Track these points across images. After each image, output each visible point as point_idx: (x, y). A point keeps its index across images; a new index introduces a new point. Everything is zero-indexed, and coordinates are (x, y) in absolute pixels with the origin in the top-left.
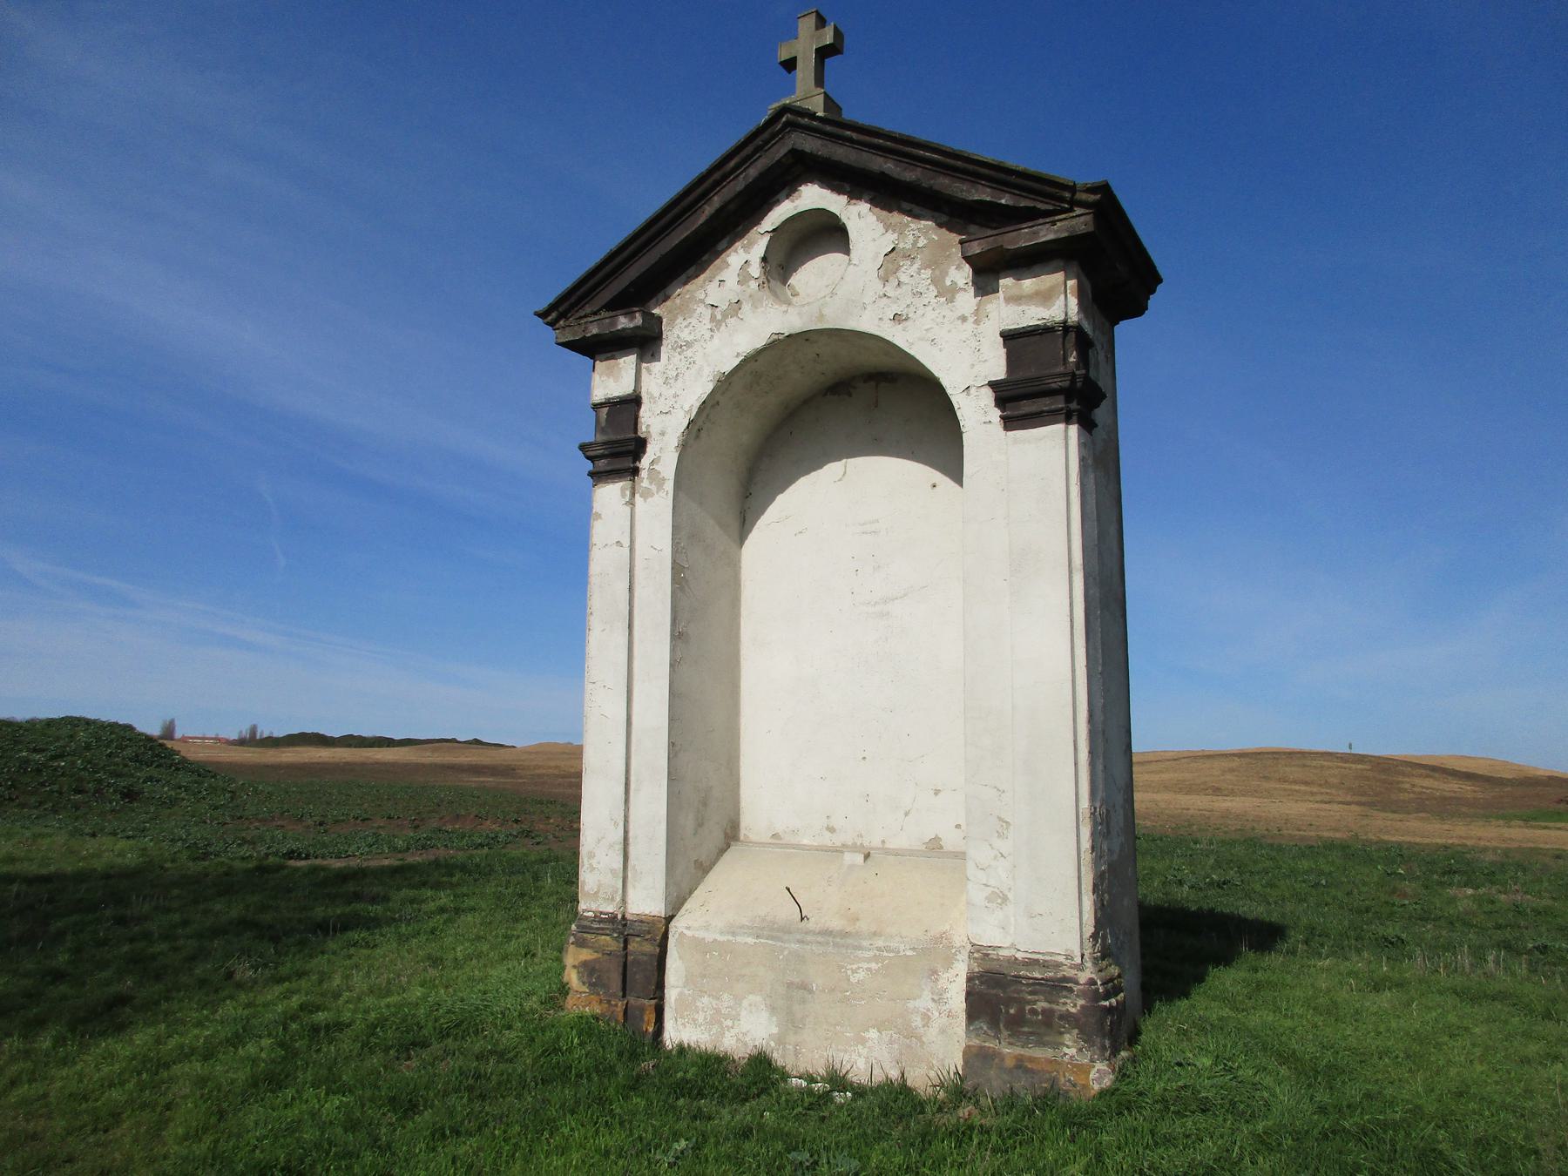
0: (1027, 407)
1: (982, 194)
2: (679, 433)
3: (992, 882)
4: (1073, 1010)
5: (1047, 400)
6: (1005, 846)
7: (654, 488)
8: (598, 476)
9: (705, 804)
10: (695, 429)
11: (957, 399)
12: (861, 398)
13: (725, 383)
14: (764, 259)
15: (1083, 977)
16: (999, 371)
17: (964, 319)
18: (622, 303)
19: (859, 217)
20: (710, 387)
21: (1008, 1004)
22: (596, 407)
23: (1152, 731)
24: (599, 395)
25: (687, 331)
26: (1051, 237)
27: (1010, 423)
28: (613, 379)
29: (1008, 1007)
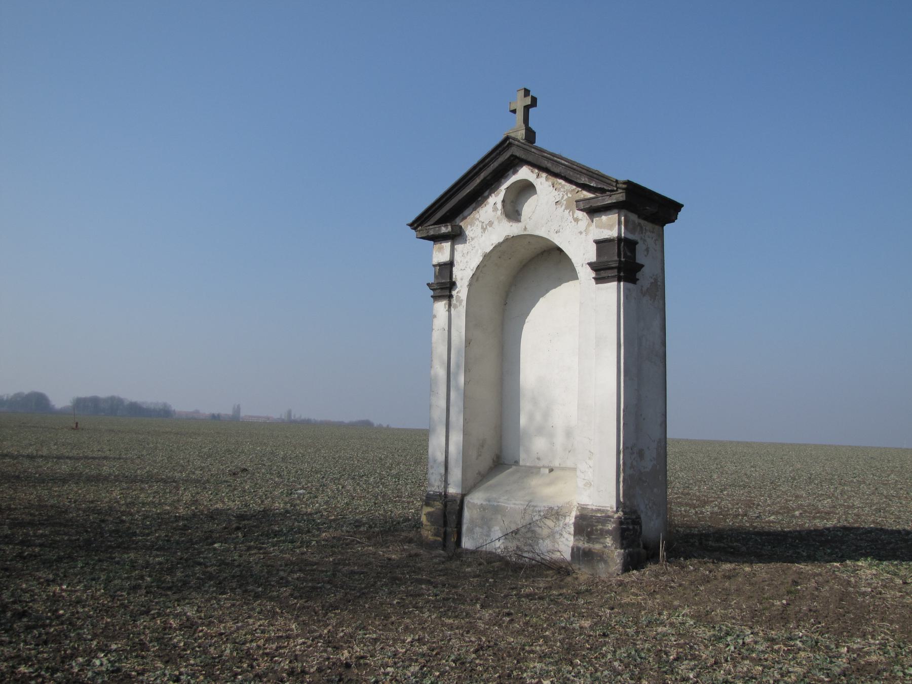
0: (603, 274)
5: (609, 271)
6: (591, 463)
8: (436, 298)
9: (483, 446)
10: (475, 278)
13: (487, 257)
14: (503, 201)
15: (616, 516)
17: (581, 233)
18: (443, 221)
19: (542, 183)
20: (481, 259)
21: (587, 527)
22: (434, 266)
23: (688, 419)
24: (435, 261)
28: (441, 253)
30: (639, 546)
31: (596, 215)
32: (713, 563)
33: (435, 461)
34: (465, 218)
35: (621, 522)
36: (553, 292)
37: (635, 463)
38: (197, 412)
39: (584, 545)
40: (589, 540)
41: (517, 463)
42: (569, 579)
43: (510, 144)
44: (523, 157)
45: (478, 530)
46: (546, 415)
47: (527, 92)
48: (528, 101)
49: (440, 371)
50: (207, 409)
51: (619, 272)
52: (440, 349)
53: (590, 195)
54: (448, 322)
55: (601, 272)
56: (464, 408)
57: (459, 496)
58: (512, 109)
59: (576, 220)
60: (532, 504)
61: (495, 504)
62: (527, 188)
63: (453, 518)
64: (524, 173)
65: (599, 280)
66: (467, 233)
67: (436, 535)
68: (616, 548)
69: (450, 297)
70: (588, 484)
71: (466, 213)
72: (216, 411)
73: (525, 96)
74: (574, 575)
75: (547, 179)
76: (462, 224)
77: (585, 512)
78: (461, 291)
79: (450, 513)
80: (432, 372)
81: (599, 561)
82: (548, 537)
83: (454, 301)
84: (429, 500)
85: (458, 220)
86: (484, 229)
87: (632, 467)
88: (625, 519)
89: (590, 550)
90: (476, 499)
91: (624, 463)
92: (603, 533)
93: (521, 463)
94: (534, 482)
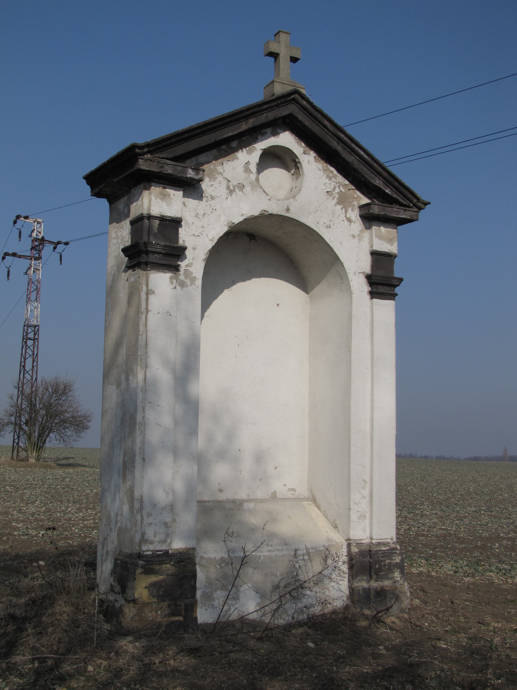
1: (378, 182)
3: (360, 510)
4: (398, 561)
11: (351, 276)
12: (265, 247)
16: (368, 270)
19: (309, 160)
27: (373, 295)
29: (375, 565)
33: (154, 506)
69: (176, 269)
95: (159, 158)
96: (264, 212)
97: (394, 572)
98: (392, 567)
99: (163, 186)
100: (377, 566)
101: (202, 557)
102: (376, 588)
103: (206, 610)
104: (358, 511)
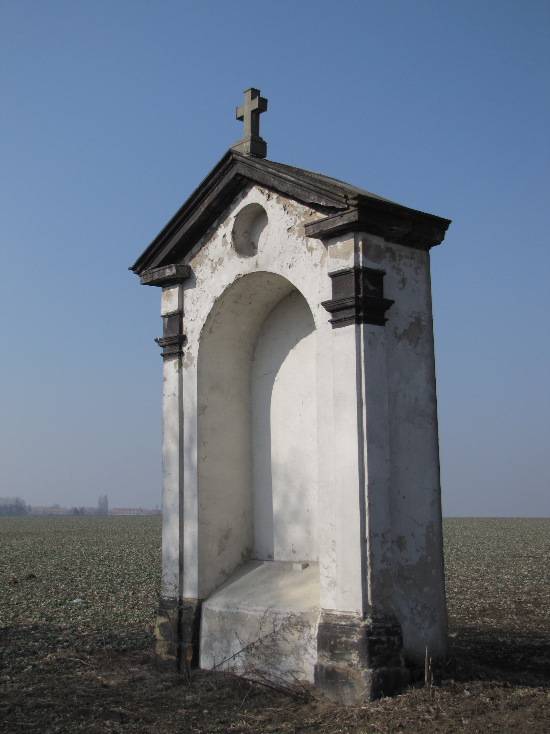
0: (341, 315)
2: (199, 332)
3: (330, 575)
4: (356, 641)
5: (347, 311)
7: (189, 362)
8: (166, 356)
9: (226, 538)
13: (218, 302)
14: (233, 232)
15: (363, 624)
17: (316, 265)
18: (165, 263)
19: (273, 207)
20: (212, 305)
22: (163, 317)
24: (163, 312)
25: (201, 273)
26: (341, 223)
28: (169, 301)
30: (398, 663)
31: (330, 241)
32: (505, 686)
33: (169, 558)
34: (193, 256)
35: (368, 632)
36: (304, 341)
37: (389, 555)
38: (57, 507)
39: (328, 663)
40: (334, 657)
41: (270, 557)
42: (305, 708)
43: (234, 161)
44: (249, 175)
45: (217, 644)
46: (302, 496)
47: (255, 93)
48: (255, 104)
49: (171, 446)
50: (68, 501)
51: (358, 312)
52: (172, 420)
53: (320, 216)
54: (177, 383)
55: (338, 312)
56: (199, 491)
57: (196, 602)
58: (239, 116)
59: (311, 250)
60: (275, 610)
61: (235, 611)
62: (258, 215)
63: (188, 630)
64: (254, 196)
65: (336, 323)
66: (196, 274)
67: (170, 652)
68: (363, 667)
70: (333, 583)
71: (194, 250)
72: (78, 505)
73: (253, 98)
74: (313, 704)
75: (278, 202)
76: (191, 264)
77: (329, 619)
78: (192, 347)
79: (186, 624)
80: (164, 448)
81: (344, 684)
82: (292, 652)
83: (185, 360)
84: (163, 608)
85: (186, 259)
86: (214, 269)
87: (385, 559)
88: (374, 628)
89: (333, 669)
90: (215, 605)
91: (372, 555)
92: (348, 647)
93: (276, 558)
94: (284, 582)
95: (153, 269)
96: (238, 276)
97: (351, 653)
98: (349, 647)
99: (168, 288)
100: (332, 643)
101: (207, 609)
102: (327, 668)
103: (207, 657)
104: (327, 577)
